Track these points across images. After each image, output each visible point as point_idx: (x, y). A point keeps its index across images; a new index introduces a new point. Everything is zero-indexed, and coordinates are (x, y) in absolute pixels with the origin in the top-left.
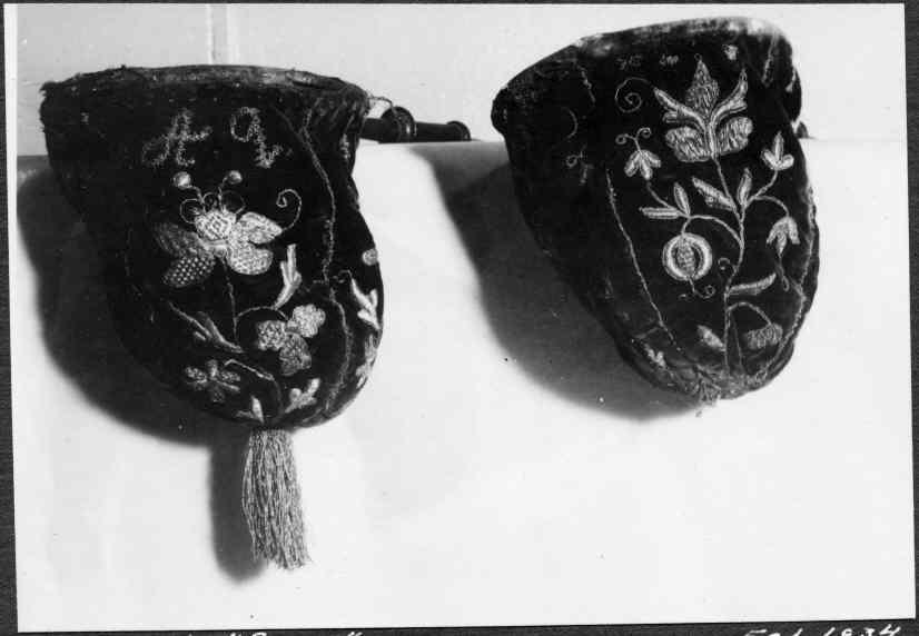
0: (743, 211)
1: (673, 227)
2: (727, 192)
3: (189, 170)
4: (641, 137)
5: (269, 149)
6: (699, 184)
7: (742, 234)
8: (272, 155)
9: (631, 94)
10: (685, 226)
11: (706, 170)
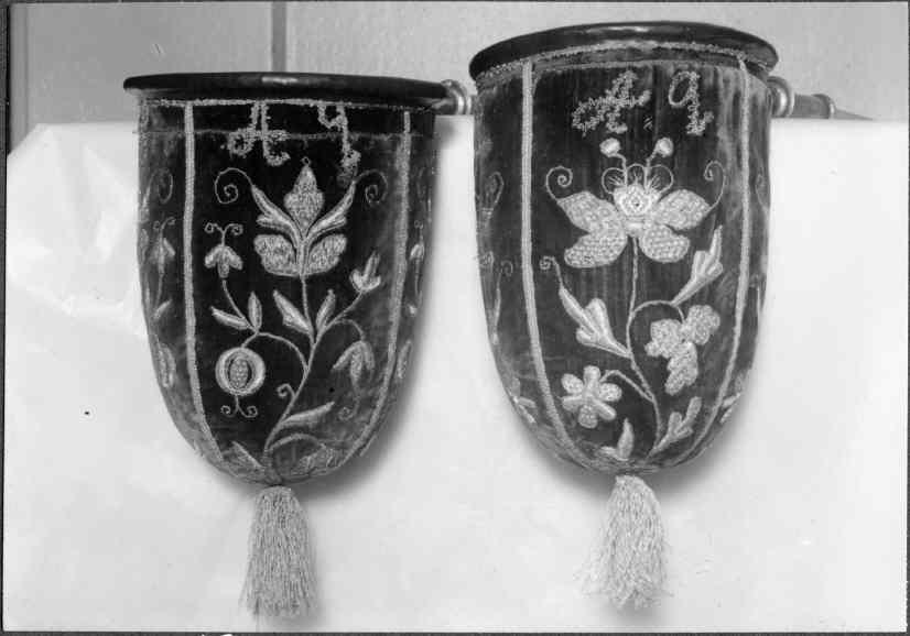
0: (320, 335)
1: (234, 337)
2: (306, 314)
3: (620, 137)
4: (229, 232)
5: (701, 116)
6: (282, 302)
7: (310, 361)
8: (703, 123)
9: (232, 186)
10: (248, 341)
11: (291, 288)
